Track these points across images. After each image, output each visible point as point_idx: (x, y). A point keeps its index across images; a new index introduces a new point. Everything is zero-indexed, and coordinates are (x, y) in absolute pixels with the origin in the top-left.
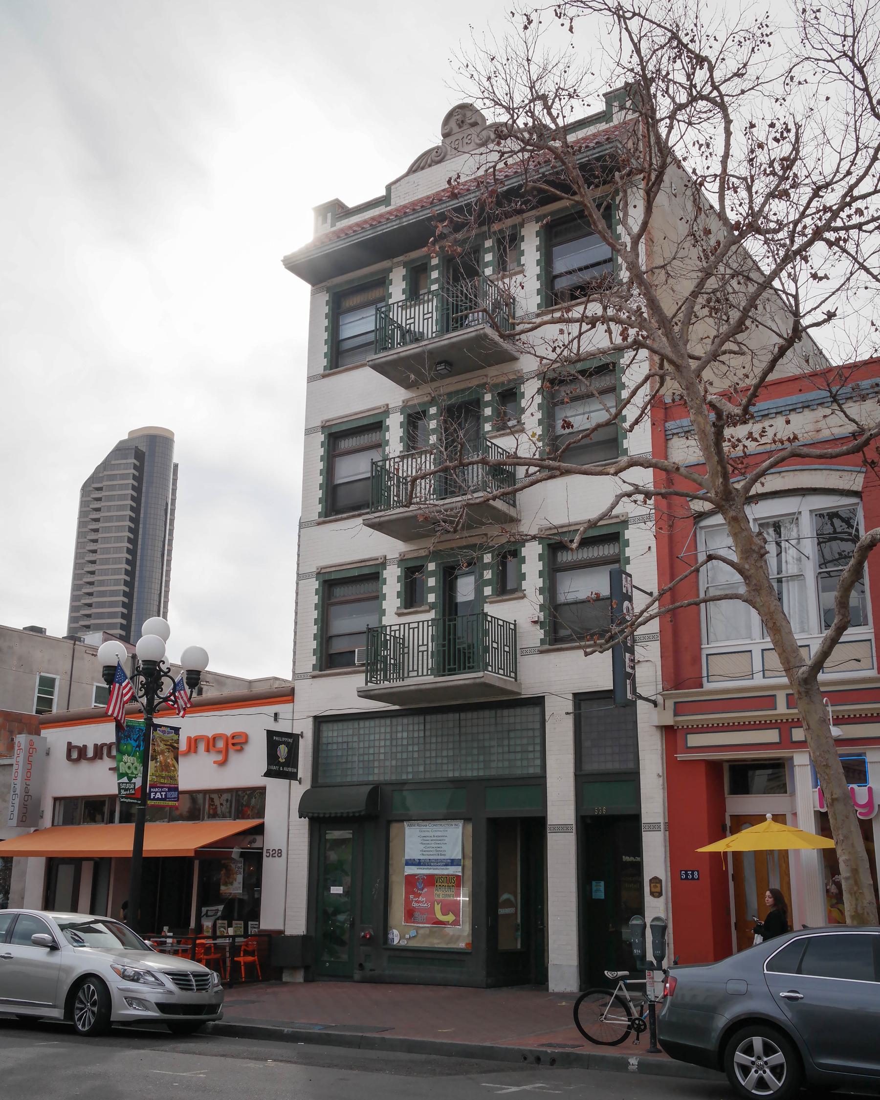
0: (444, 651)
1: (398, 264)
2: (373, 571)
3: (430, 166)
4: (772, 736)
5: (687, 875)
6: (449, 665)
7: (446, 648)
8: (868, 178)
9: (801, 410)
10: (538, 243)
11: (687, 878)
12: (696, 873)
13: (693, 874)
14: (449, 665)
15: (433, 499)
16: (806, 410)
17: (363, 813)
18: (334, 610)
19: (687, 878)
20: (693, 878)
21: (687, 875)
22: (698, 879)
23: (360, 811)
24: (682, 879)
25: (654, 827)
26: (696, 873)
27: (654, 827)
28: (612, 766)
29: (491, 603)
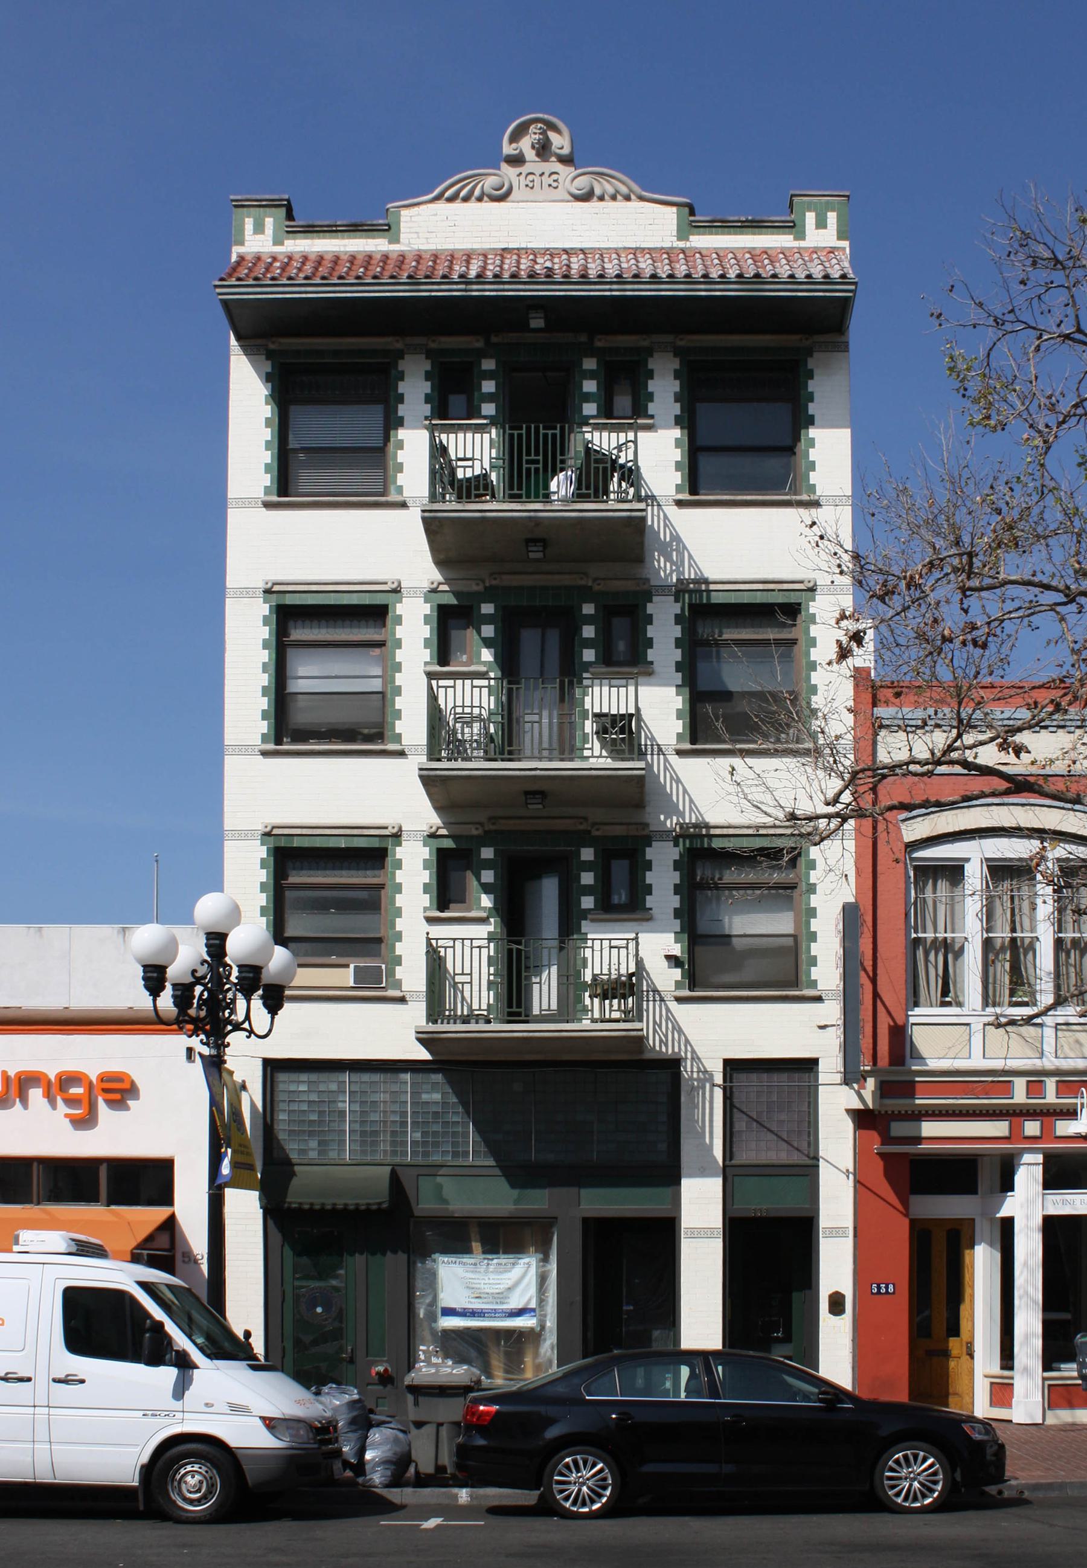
0: (562, 453)
1: (415, 350)
2: (377, 845)
3: (480, 199)
4: (999, 1128)
5: (879, 1288)
6: (528, 454)
7: (559, 457)
8: (624, 827)
9: (1054, 729)
10: (678, 389)
11: (879, 1292)
12: (891, 1287)
13: (887, 1288)
14: (528, 454)
15: (450, 501)
16: (1060, 730)
17: (385, 1206)
18: (700, 896)
19: (879, 1292)
20: (887, 1292)
21: (879, 1288)
22: (894, 1293)
23: (380, 1204)
24: (872, 1293)
25: (836, 1232)
26: (891, 1287)
27: (836, 1232)
28: (780, 1155)
29: (593, 921)
